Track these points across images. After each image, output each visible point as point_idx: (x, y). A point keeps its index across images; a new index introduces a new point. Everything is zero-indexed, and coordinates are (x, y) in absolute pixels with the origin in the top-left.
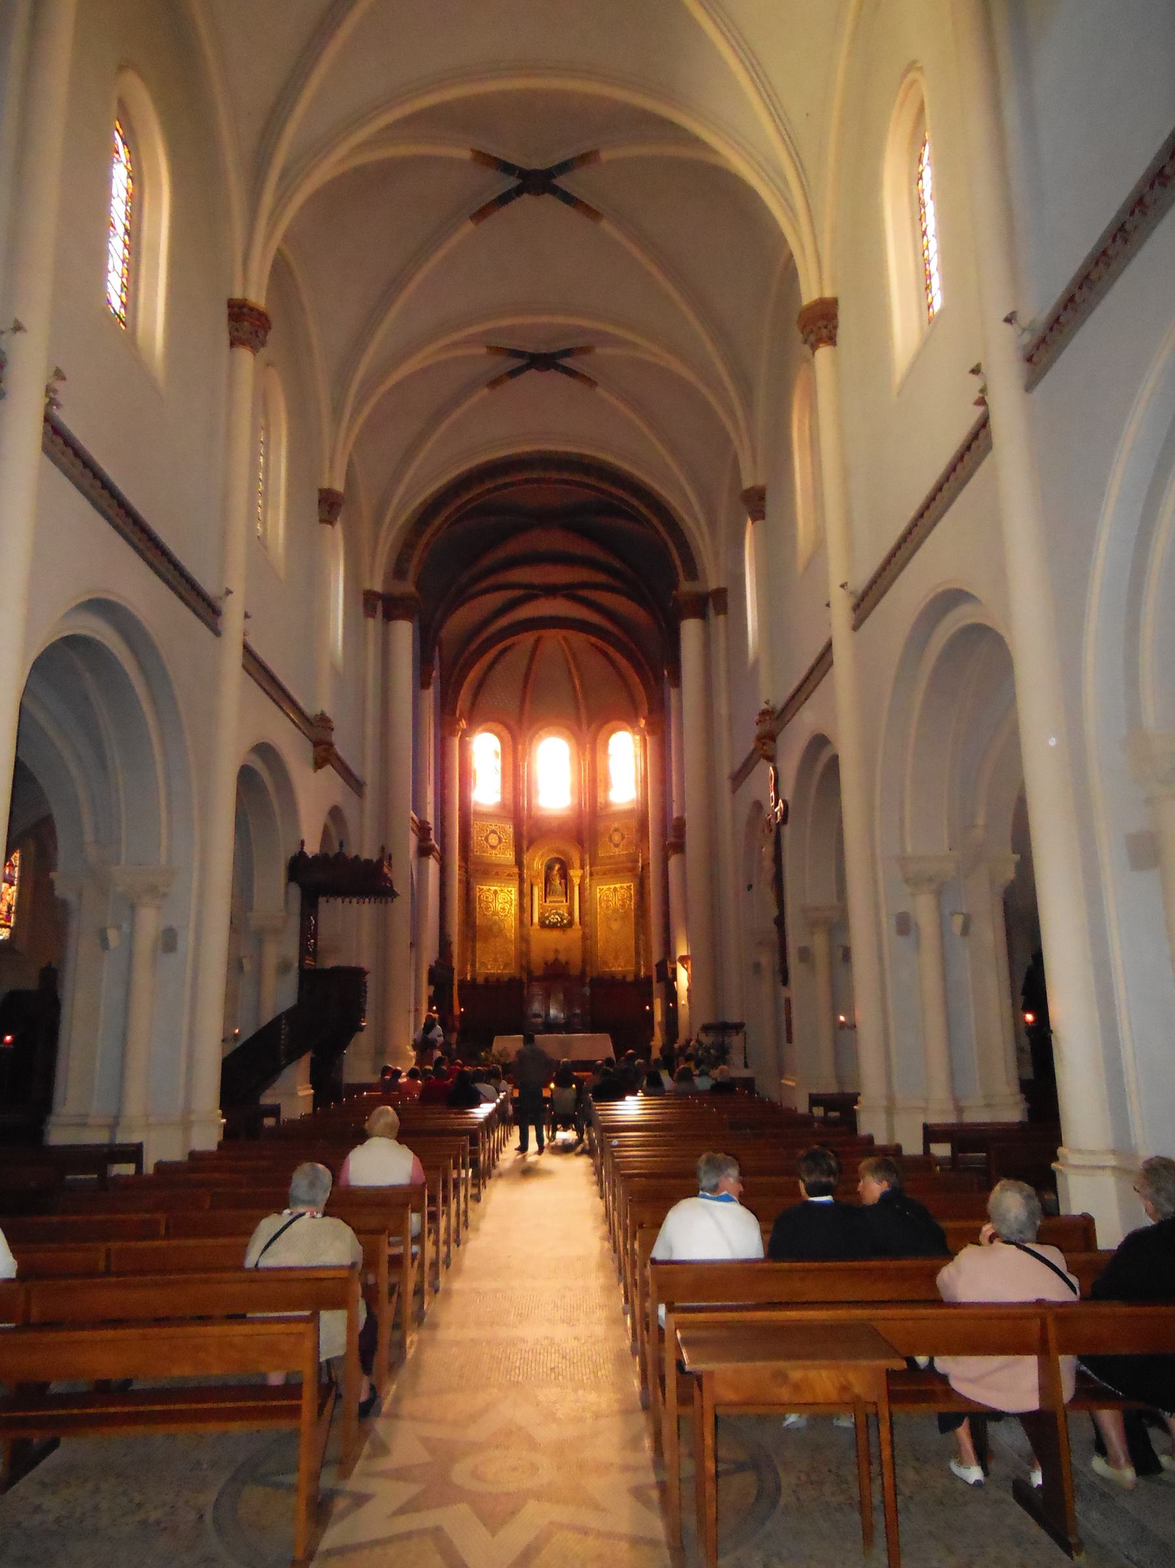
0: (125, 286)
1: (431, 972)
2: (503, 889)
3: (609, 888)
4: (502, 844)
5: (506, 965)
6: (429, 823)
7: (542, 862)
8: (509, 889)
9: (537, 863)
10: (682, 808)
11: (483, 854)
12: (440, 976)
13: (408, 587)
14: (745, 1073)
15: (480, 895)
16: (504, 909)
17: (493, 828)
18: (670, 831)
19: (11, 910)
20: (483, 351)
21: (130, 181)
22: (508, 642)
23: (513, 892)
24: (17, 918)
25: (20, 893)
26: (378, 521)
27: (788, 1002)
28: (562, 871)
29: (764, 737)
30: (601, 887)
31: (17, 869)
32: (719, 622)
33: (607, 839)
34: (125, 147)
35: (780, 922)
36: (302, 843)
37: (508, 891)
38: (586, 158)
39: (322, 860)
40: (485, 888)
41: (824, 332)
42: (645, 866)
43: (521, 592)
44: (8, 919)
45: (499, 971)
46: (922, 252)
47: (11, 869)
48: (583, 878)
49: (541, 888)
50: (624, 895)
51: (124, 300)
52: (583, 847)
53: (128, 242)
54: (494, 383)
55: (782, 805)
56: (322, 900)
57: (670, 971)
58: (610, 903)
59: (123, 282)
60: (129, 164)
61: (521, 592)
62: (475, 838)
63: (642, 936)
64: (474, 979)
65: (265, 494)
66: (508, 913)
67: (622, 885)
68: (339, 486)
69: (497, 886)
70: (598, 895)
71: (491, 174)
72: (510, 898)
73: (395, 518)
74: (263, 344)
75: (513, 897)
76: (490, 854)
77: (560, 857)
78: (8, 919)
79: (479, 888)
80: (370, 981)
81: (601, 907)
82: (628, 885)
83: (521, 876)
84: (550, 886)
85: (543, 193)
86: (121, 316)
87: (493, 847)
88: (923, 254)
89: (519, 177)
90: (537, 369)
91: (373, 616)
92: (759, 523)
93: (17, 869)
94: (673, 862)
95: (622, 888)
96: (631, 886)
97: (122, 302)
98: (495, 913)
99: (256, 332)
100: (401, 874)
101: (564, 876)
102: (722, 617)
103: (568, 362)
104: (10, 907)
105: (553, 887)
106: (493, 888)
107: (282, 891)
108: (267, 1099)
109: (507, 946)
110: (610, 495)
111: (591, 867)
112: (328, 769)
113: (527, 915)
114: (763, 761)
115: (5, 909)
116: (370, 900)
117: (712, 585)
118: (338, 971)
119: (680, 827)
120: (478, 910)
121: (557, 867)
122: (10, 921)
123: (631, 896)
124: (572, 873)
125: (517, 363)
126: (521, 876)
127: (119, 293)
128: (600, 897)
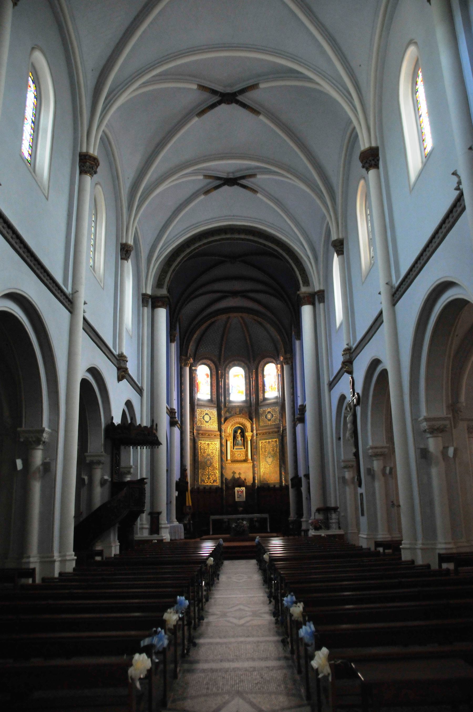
0: (31, 147)
1: (177, 484)
2: (212, 443)
4: (211, 420)
6: (175, 409)
7: (232, 429)
8: (215, 443)
9: (229, 429)
10: (304, 399)
11: (202, 425)
13: (164, 292)
14: (341, 532)
15: (201, 446)
16: (213, 453)
17: (207, 412)
18: (297, 412)
21: (35, 99)
22: (213, 320)
23: (217, 444)
28: (241, 434)
30: (262, 441)
34: (34, 84)
35: (356, 455)
36: (112, 418)
37: (215, 444)
40: (203, 442)
41: (373, 162)
42: (284, 430)
43: (219, 295)
46: (420, 125)
48: (252, 436)
50: (273, 445)
51: (30, 153)
53: (33, 127)
54: (207, 192)
55: (357, 396)
56: (122, 447)
58: (267, 449)
59: (30, 145)
60: (35, 92)
61: (219, 295)
62: (198, 417)
63: (283, 465)
65: (94, 246)
66: (215, 454)
67: (272, 440)
68: (131, 242)
69: (209, 441)
70: (260, 445)
71: (206, 95)
72: (216, 447)
74: (96, 173)
75: (217, 447)
76: (205, 425)
77: (241, 426)
79: (200, 442)
82: (276, 440)
83: (221, 436)
84: (236, 441)
86: (29, 160)
87: (207, 422)
88: (421, 126)
89: (220, 96)
90: (228, 185)
91: (147, 306)
92: (340, 256)
94: (299, 427)
95: (272, 441)
96: (277, 440)
97: (29, 154)
98: (208, 455)
101: (243, 435)
102: (322, 305)
103: (243, 182)
105: (237, 442)
106: (207, 442)
109: (214, 471)
110: (265, 245)
111: (256, 431)
112: (125, 381)
113: (224, 456)
114: (346, 374)
116: (140, 447)
117: (317, 289)
119: (303, 409)
120: (200, 453)
121: (239, 431)
123: (277, 446)
124: (247, 434)
125: (218, 182)
126: (221, 436)
127: (28, 150)
128: (262, 445)
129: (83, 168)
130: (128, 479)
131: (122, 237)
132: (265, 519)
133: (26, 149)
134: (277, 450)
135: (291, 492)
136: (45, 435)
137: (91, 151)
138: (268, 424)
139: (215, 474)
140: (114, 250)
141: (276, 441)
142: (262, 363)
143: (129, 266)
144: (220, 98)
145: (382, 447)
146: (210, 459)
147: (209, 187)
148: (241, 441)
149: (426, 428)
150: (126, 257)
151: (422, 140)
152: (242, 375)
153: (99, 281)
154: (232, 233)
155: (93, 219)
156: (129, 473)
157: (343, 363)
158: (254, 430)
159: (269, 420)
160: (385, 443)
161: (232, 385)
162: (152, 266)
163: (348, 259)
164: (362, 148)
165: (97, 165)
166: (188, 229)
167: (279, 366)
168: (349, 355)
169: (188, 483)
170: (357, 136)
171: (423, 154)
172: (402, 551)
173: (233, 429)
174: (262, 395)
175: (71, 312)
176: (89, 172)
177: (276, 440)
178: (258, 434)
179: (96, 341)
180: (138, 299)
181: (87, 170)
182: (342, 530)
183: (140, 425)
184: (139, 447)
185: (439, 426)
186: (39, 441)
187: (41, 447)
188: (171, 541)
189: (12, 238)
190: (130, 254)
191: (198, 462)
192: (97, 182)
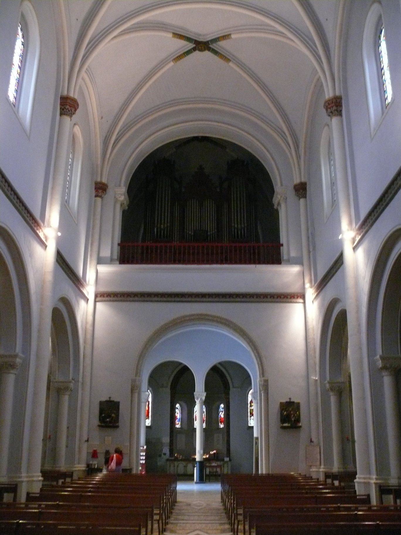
20: (172, 64)
21: (22, 46)
38: (226, 37)
51: (15, 96)
68: (104, 181)
85: (205, 50)
97: (14, 97)
133: (11, 93)
137: (71, 95)
144: (194, 46)
151: (382, 91)
158: (198, 451)
164: (295, 183)
170: (322, 86)
171: (384, 104)
186: (13, 366)
187: (68, 393)
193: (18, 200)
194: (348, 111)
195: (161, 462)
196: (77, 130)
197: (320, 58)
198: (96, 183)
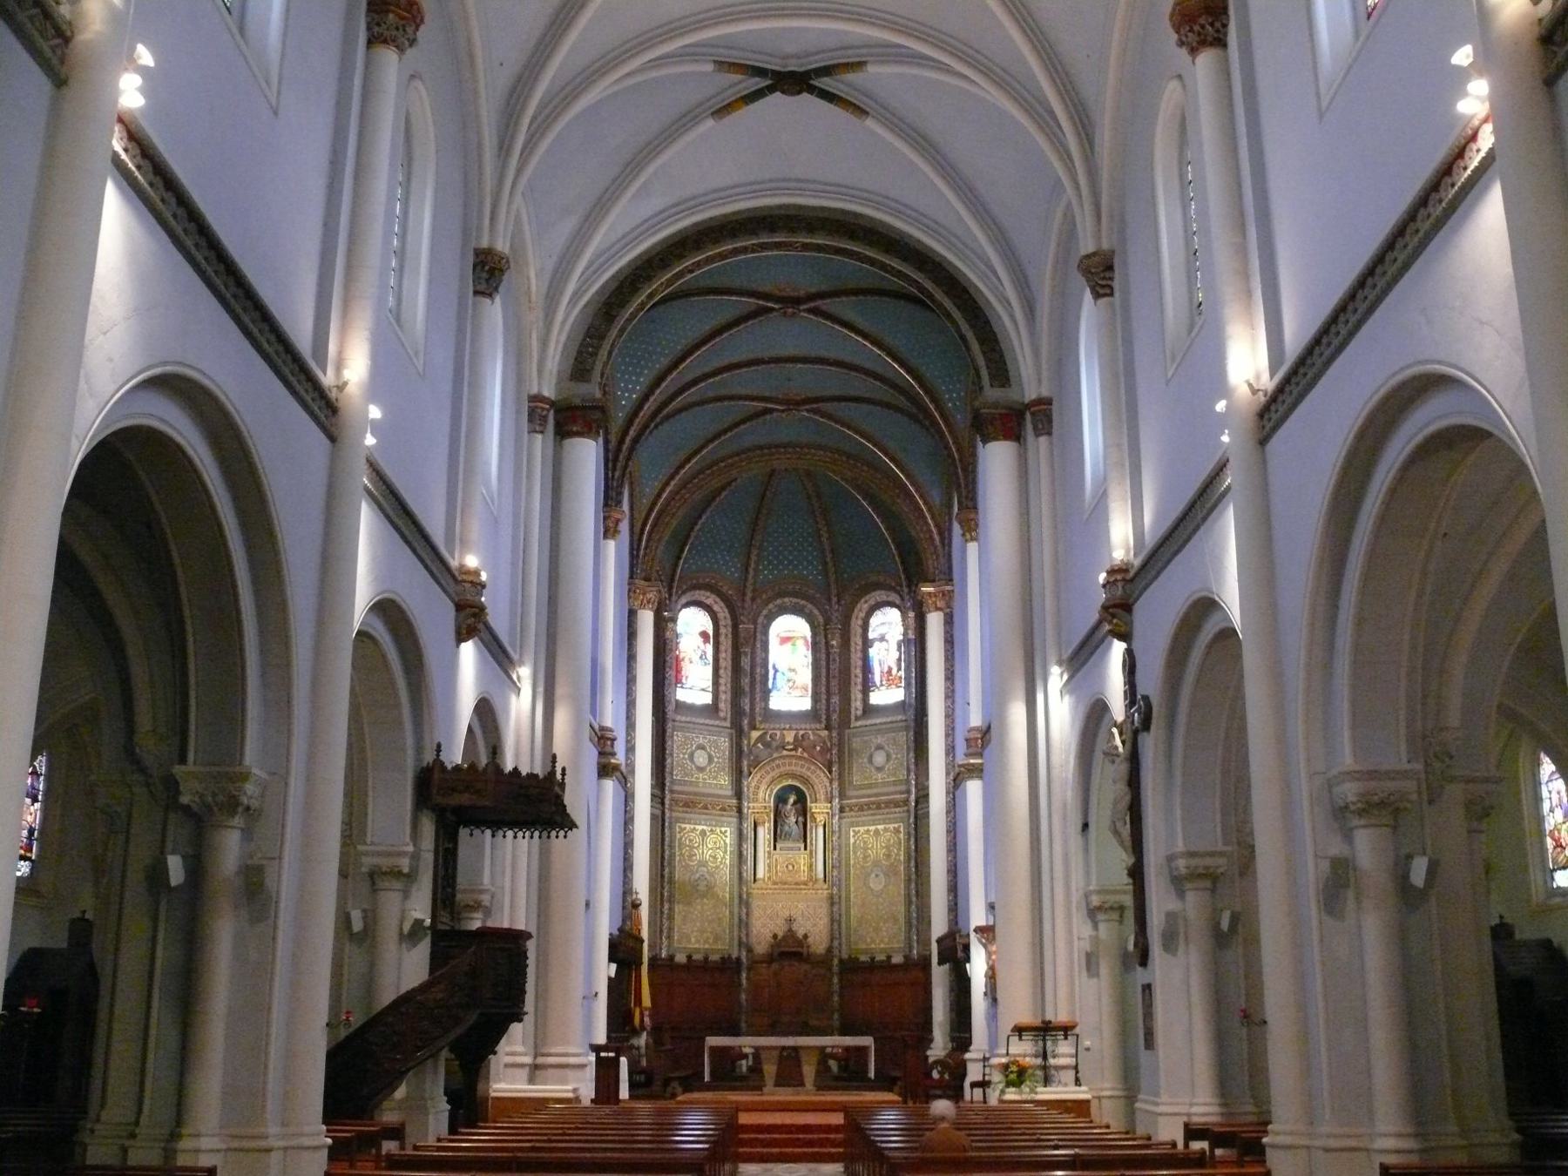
3: (868, 830)
5: (717, 939)
7: (772, 791)
8: (723, 829)
12: (623, 949)
16: (715, 857)
19: (33, 835)
20: (709, 67)
24: (40, 849)
25: (46, 811)
26: (552, 299)
27: (1147, 988)
29: (1115, 606)
30: (857, 829)
31: (42, 778)
32: (1040, 446)
33: (865, 760)
35: (1137, 873)
39: (467, 776)
44: (29, 848)
45: (707, 946)
47: (35, 777)
49: (769, 830)
52: (830, 772)
56: (463, 833)
57: (960, 948)
64: (671, 958)
65: (401, 254)
66: (721, 862)
67: (887, 826)
68: (502, 246)
73: (576, 295)
75: (728, 841)
78: (29, 848)
80: (531, 946)
81: (856, 857)
82: (896, 825)
83: (740, 811)
87: (701, 769)
90: (783, 92)
93: (42, 778)
95: (886, 830)
98: (703, 863)
99: (404, 26)
100: (575, 801)
101: (803, 810)
102: (1043, 440)
103: (824, 83)
104: (31, 831)
105: (787, 828)
106: (700, 828)
107: (408, 817)
108: (389, 1116)
115: (25, 833)
116: (541, 833)
117: (1030, 394)
118: (486, 934)
120: (677, 858)
122: (31, 851)
129: (376, 29)
130: (476, 925)
131: (479, 228)
132: (862, 1051)
134: (898, 854)
135: (940, 976)
136: (250, 788)
138: (876, 779)
139: (719, 919)
140: (458, 270)
141: (897, 831)
142: (863, 606)
143: (494, 311)
145: (1212, 854)
146: (707, 876)
147: (730, 95)
148: (795, 826)
149: (1351, 798)
150: (488, 289)
152: (805, 638)
153: (411, 353)
154: (792, 231)
155: (401, 179)
156: (477, 906)
157: (1105, 608)
159: (879, 769)
160: (1220, 844)
161: (774, 667)
162: (560, 316)
163: (1126, 308)
165: (418, 21)
166: (635, 233)
167: (911, 614)
168: (1123, 587)
169: (642, 941)
172: (1268, 1150)
173: (775, 792)
174: (860, 696)
175: (332, 439)
176: (394, 41)
177: (896, 825)
178: (847, 809)
179: (400, 523)
180: (518, 412)
181: (386, 33)
182: (1083, 1088)
183: (516, 769)
184: (510, 833)
185: (1386, 794)
186: (232, 805)
187: (238, 821)
188: (593, 1105)
189: (175, 216)
190: (501, 281)
191: (671, 881)
192: (412, 73)
193: (213, 252)
194: (1245, 28)
195: (456, 599)
196: (423, 102)
197: (1071, 160)
198: (478, 253)
